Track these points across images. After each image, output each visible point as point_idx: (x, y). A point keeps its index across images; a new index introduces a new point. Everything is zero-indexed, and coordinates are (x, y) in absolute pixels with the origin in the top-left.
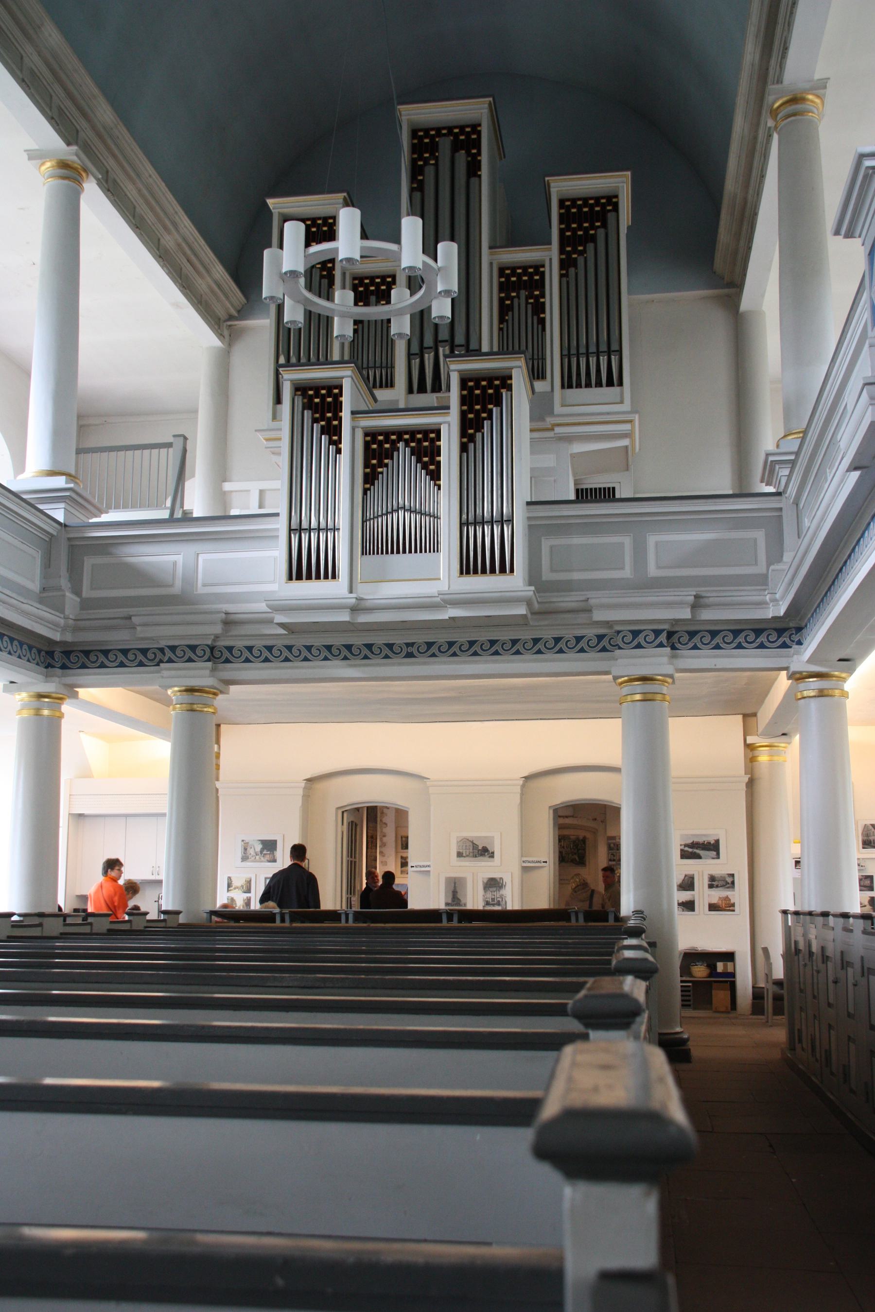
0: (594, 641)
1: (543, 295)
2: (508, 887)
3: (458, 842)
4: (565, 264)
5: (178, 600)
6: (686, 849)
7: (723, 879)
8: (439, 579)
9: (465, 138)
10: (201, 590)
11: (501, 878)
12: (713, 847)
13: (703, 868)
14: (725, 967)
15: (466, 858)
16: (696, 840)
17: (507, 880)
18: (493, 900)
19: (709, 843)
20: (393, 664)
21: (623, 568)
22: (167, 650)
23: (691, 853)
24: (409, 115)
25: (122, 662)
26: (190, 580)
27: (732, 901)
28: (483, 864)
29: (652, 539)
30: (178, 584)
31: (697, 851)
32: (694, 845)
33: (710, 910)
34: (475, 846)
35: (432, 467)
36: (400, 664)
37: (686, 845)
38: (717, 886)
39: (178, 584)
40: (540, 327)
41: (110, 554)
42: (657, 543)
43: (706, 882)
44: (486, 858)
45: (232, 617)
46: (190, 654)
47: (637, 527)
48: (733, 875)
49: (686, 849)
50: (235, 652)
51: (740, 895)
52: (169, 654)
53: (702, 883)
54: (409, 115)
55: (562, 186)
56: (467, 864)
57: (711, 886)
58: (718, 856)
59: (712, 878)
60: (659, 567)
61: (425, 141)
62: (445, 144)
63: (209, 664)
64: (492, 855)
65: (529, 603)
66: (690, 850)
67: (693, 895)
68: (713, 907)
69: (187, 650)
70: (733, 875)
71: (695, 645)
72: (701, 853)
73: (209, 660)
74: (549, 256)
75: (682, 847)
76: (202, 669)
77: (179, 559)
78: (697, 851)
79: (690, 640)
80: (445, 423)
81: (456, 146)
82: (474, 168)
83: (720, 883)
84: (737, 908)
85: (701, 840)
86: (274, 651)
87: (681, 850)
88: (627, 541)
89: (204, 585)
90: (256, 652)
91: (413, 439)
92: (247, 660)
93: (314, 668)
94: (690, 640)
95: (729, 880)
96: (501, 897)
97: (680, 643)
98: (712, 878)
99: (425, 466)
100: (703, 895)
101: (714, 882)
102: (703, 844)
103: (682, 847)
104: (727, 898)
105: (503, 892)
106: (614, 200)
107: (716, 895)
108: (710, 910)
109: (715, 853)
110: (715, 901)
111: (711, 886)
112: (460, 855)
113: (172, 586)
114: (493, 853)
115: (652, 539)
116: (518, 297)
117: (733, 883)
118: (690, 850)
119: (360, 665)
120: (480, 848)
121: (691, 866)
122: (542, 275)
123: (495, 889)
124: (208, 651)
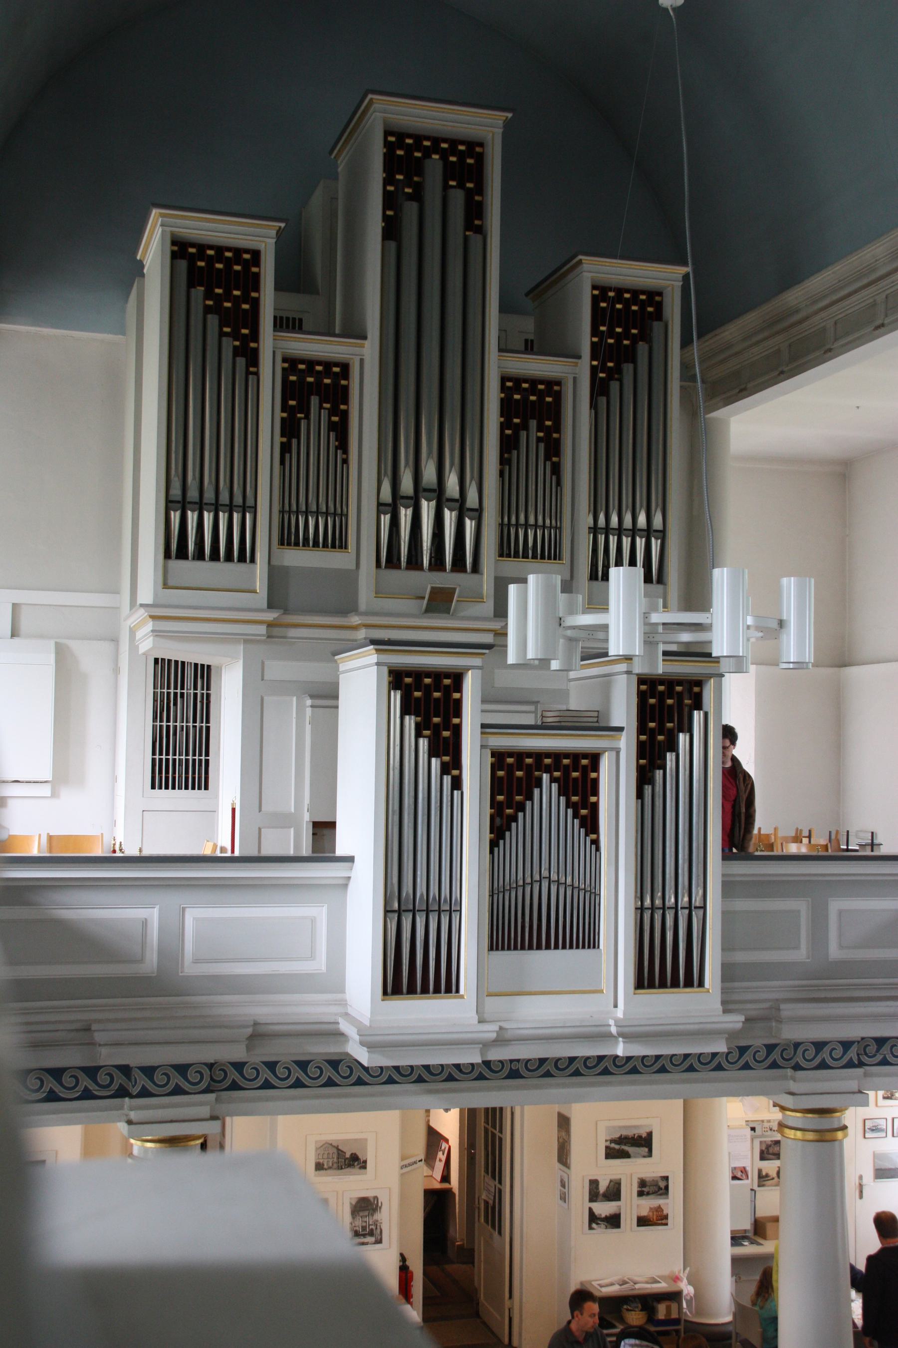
0: (763, 1053)
1: (557, 427)
2: (385, 1209)
3: (317, 1149)
4: (599, 389)
5: (157, 989)
6: (613, 1145)
7: (655, 1183)
8: (601, 991)
9: (464, 162)
10: (190, 968)
11: (376, 1198)
12: (644, 1142)
13: (631, 1170)
14: (669, 1309)
15: (329, 1172)
16: (625, 1133)
17: (383, 1199)
18: (364, 1228)
19: (640, 1137)
20: (489, 1089)
21: (797, 947)
22: (137, 1074)
23: (618, 1150)
24: (385, 112)
25: (51, 1091)
26: (171, 952)
27: (665, 1212)
28: (352, 1178)
29: (835, 905)
30: (152, 960)
31: (626, 1148)
32: (622, 1140)
33: (639, 1225)
34: (340, 1152)
35: (584, 812)
36: (500, 1089)
37: (612, 1141)
38: (648, 1194)
39: (152, 960)
40: (554, 478)
41: (28, 903)
42: (840, 913)
43: (635, 1189)
44: (356, 1170)
45: (262, 1029)
46: (177, 1079)
47: (818, 891)
48: (666, 1178)
49: (613, 1145)
50: (247, 1071)
51: (673, 1204)
52: (142, 1081)
53: (629, 1190)
54: (385, 112)
55: (597, 270)
56: (329, 1179)
57: (641, 1194)
58: (650, 1154)
59: (642, 1183)
60: (841, 947)
61: (406, 155)
62: (434, 164)
63: (211, 1097)
64: (364, 1166)
65: (731, 1035)
66: (617, 1147)
67: (619, 1207)
68: (643, 1222)
69: (173, 1073)
70: (666, 1178)
71: (885, 1058)
72: (630, 1150)
73: (207, 1091)
74: (575, 373)
75: (608, 1144)
76: (201, 1104)
77: (153, 915)
78: (626, 1148)
79: (878, 1051)
80: (612, 749)
81: (449, 171)
82: (475, 212)
83: (652, 1189)
84: (670, 1221)
85: (630, 1133)
86: (311, 1069)
87: (607, 1147)
88: (801, 906)
89: (196, 961)
90: (281, 1071)
91: (557, 765)
92: (267, 1085)
93: (372, 1095)
94: (878, 1051)
95: (662, 1184)
96: (376, 1223)
97: (866, 1054)
98: (642, 1183)
99: (575, 807)
100: (631, 1205)
101: (646, 1188)
102: (633, 1138)
103: (608, 1144)
104: (659, 1209)
105: (377, 1216)
106: (657, 298)
107: (645, 1206)
108: (639, 1225)
109: (646, 1150)
110: (644, 1212)
111: (641, 1194)
112: (319, 1167)
113: (142, 961)
114: (365, 1162)
115: (835, 905)
116: (526, 427)
117: (667, 1188)
118: (617, 1147)
119: (444, 1091)
120: (348, 1155)
121: (619, 1169)
122: (558, 396)
123: (366, 1213)
124: (206, 1072)
